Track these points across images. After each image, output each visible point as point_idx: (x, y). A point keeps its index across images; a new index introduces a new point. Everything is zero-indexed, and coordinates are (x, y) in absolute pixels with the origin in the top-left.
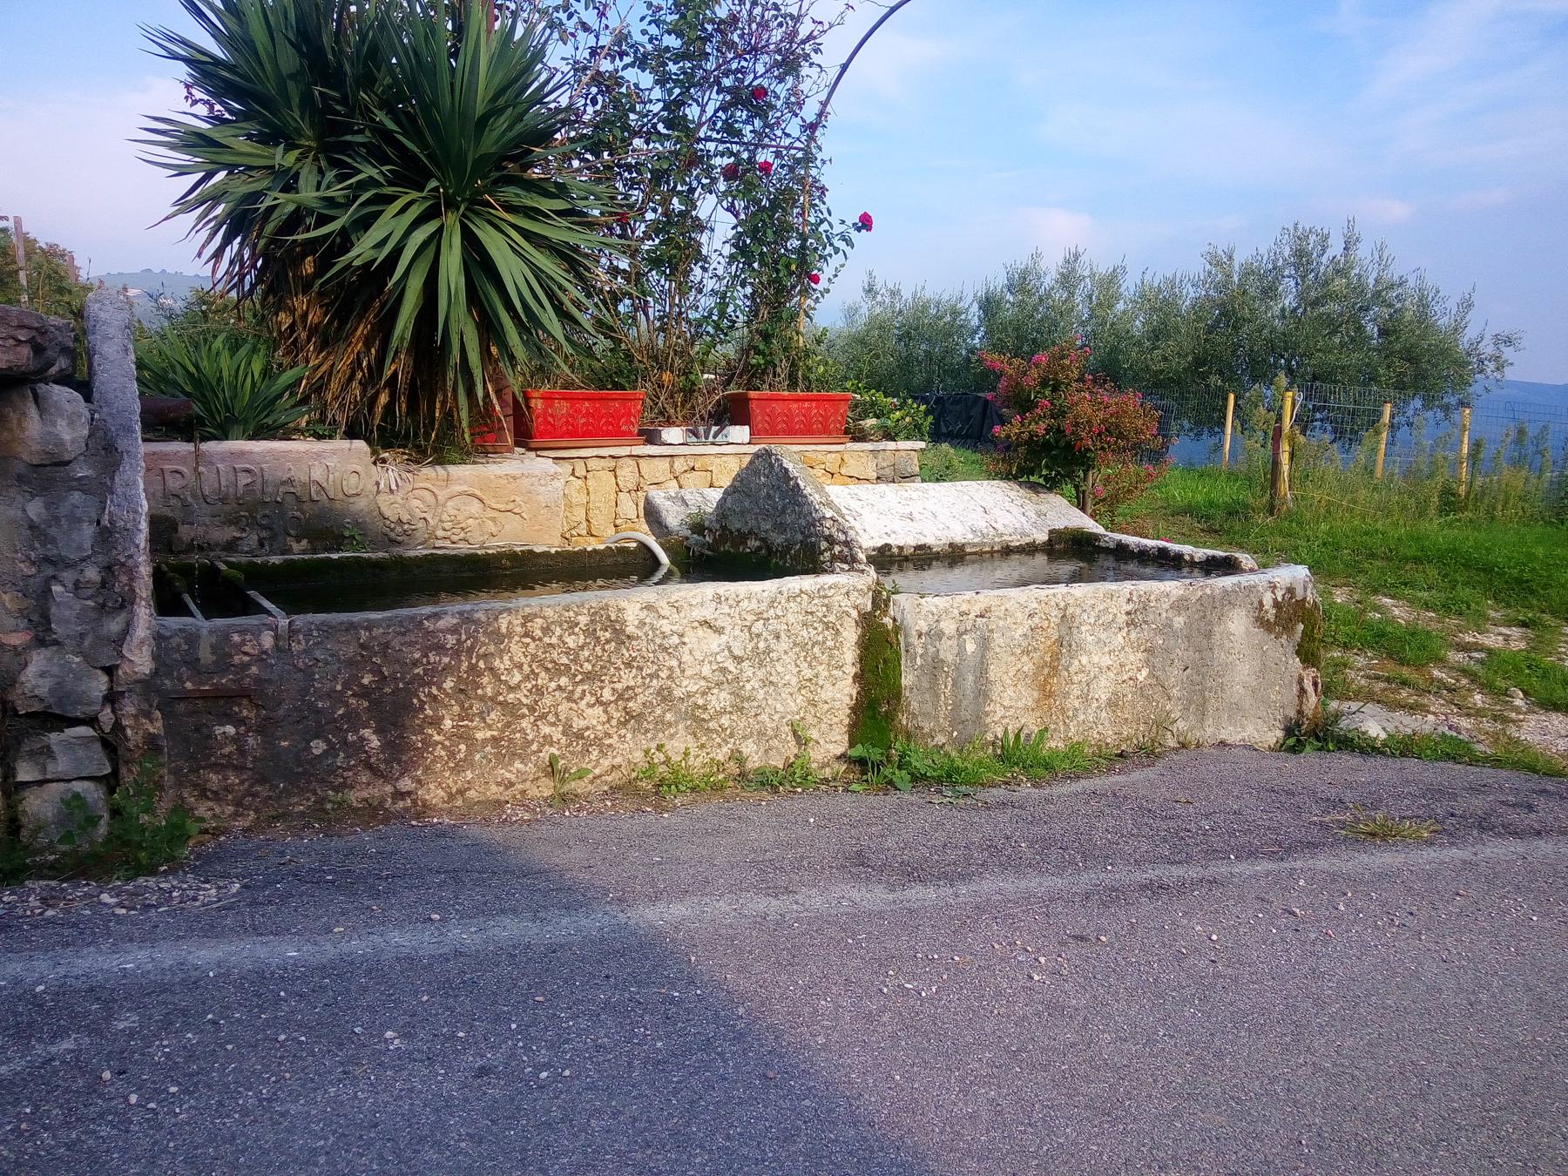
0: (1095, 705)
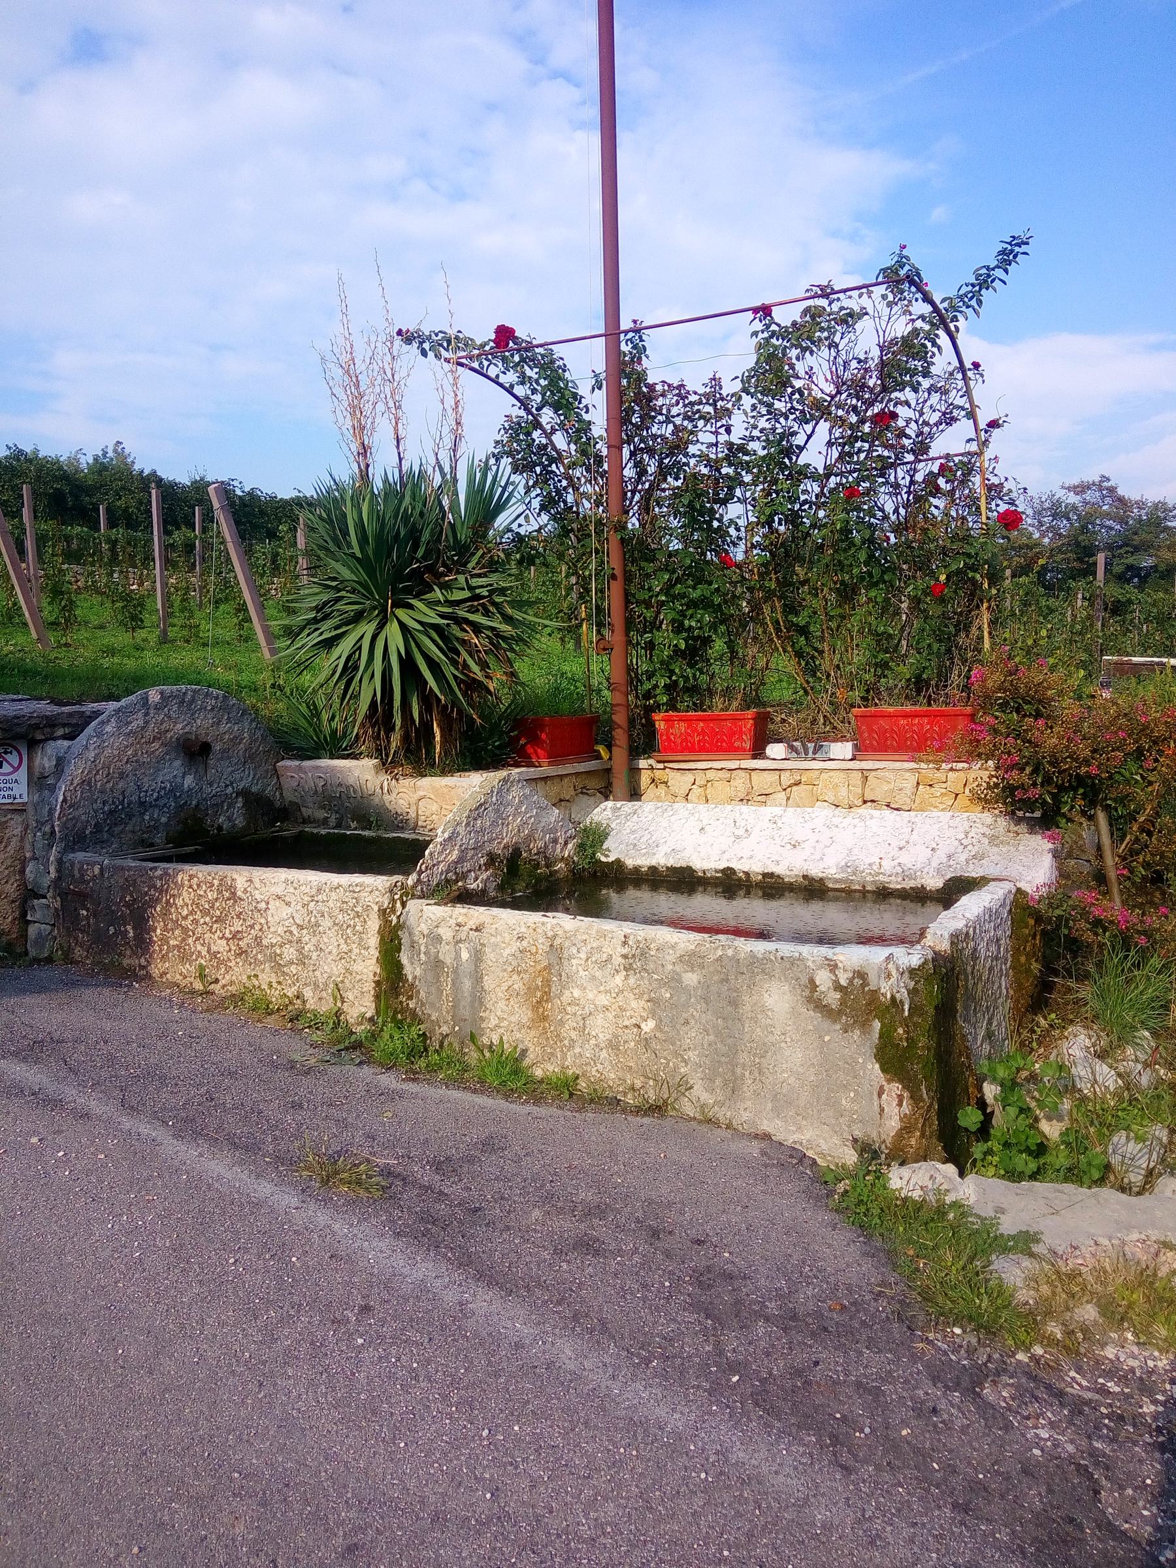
0: (593, 1042)
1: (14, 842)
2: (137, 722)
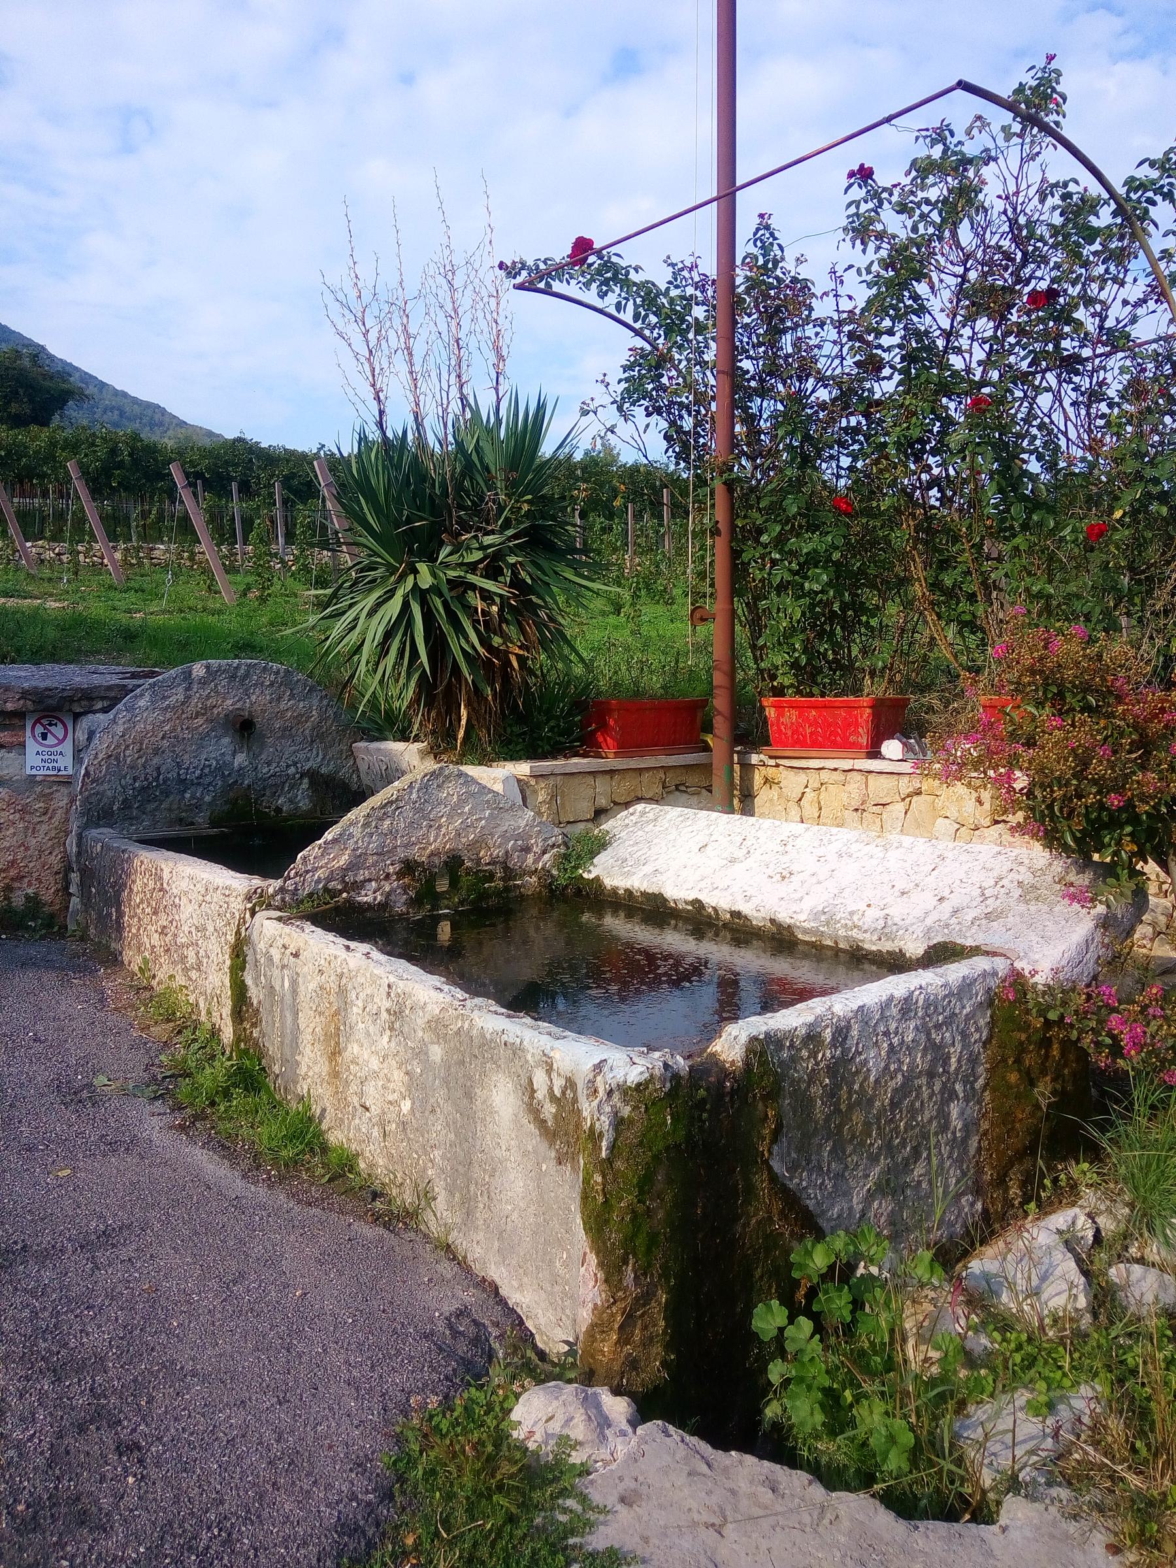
1: (59, 815)
2: (178, 695)
